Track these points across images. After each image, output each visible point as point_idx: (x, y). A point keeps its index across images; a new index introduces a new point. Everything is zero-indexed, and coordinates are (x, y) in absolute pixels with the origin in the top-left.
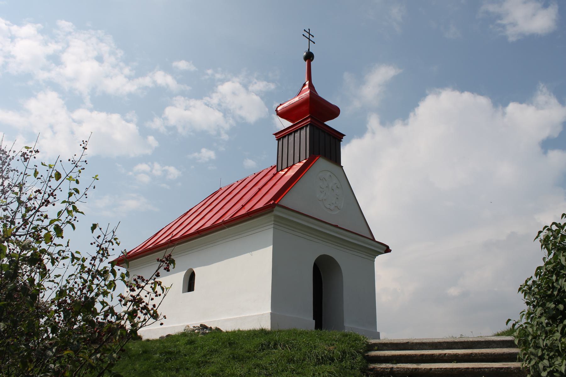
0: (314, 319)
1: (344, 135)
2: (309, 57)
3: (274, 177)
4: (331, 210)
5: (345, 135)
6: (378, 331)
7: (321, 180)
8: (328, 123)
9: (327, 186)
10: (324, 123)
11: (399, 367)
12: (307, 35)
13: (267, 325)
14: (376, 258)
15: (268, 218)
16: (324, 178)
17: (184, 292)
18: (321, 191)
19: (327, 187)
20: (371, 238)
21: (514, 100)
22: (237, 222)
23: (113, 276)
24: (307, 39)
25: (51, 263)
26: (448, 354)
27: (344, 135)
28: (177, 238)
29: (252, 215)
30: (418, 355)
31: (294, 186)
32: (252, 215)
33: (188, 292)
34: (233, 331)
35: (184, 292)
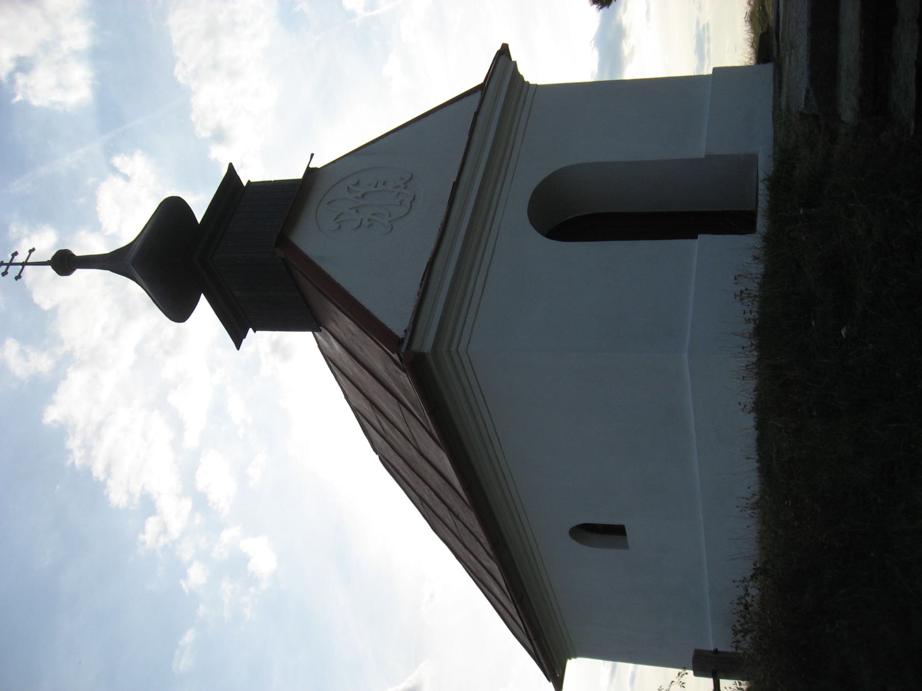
0: (696, 238)
3: (454, 509)
4: (414, 199)
7: (340, 227)
8: (199, 217)
10: (199, 223)
11: (782, 4)
12: (14, 271)
14: (528, 82)
16: (335, 220)
17: (625, 546)
18: (369, 226)
19: (357, 211)
20: (478, 95)
21: (699, 234)
25: (257, 339)
28: (505, 582)
33: (626, 535)
34: (757, 465)
35: (625, 546)
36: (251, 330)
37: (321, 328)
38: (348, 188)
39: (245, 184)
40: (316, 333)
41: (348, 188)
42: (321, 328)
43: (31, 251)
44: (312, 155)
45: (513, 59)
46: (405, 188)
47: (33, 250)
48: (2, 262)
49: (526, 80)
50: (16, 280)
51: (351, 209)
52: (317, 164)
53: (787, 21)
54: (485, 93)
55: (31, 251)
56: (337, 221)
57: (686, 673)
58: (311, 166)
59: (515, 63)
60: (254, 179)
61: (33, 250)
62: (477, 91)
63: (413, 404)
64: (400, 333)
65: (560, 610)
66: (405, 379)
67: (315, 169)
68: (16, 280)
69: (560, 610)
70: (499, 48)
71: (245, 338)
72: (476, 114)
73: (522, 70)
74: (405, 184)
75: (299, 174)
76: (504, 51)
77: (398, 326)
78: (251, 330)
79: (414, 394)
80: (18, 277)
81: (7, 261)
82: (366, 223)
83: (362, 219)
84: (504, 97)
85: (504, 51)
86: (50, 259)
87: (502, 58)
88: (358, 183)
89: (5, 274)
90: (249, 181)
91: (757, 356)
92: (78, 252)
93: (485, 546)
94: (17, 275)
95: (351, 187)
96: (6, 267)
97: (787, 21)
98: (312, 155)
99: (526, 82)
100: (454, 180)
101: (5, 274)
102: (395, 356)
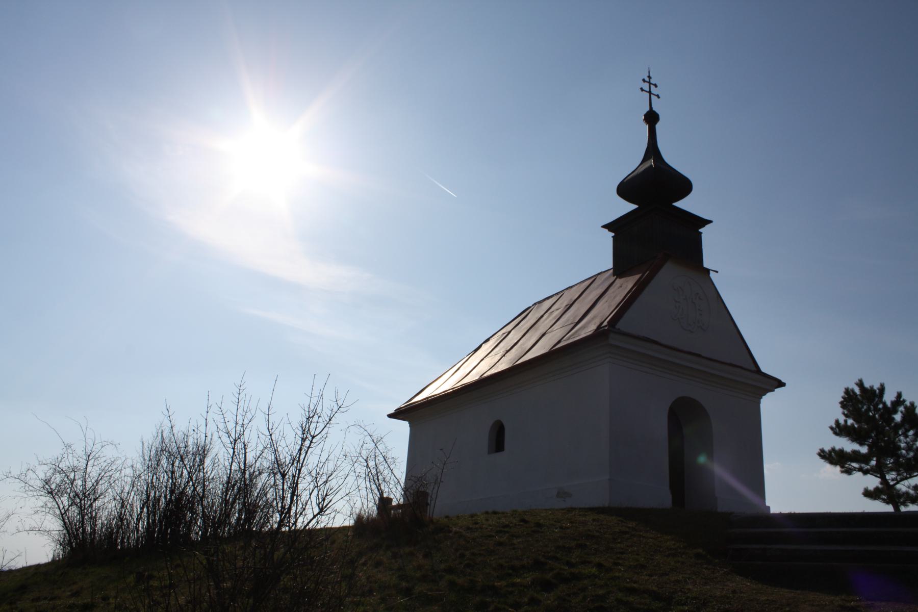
1: (705, 222)
5: (710, 222)
8: (680, 204)
12: (646, 86)
14: (762, 398)
17: (489, 453)
20: (754, 368)
27: (705, 222)
35: (489, 453)
36: (613, 234)
37: (616, 277)
39: (700, 230)
40: (612, 271)
42: (616, 277)
43: (658, 96)
44: (717, 272)
45: (777, 390)
49: (764, 397)
50: (846, 389)
52: (712, 274)
53: (297, 475)
55: (658, 96)
58: (711, 272)
59: (774, 391)
60: (703, 236)
63: (576, 332)
64: (617, 326)
66: (592, 328)
67: (709, 274)
70: (783, 381)
71: (609, 231)
72: (741, 367)
73: (769, 395)
75: (706, 264)
76: (781, 384)
77: (621, 325)
78: (613, 234)
79: (583, 335)
80: (642, 89)
85: (781, 384)
86: (654, 109)
89: (644, 81)
91: (384, 503)
92: (658, 126)
93: (489, 372)
94: (644, 88)
96: (651, 86)
97: (297, 475)
98: (717, 272)
99: (890, 503)
101: (644, 81)
102: (605, 323)
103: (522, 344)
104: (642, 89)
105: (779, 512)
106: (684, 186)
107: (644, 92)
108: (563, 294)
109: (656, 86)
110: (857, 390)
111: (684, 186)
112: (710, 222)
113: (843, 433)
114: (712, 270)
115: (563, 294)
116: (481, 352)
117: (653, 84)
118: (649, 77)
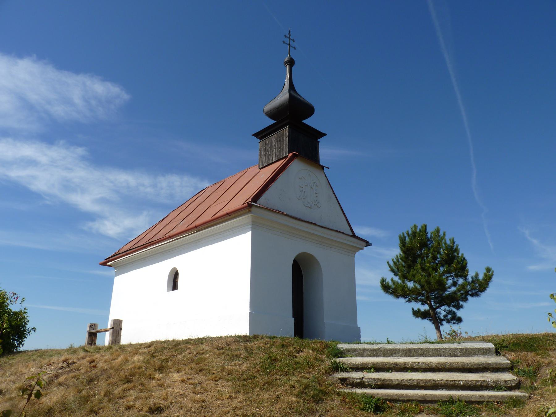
1: (322, 135)
2: (291, 62)
5: (325, 135)
6: (359, 326)
8: (306, 122)
9: (306, 184)
12: (287, 41)
13: (244, 329)
14: (356, 254)
15: (246, 218)
16: (303, 177)
17: (168, 291)
19: (306, 185)
22: (208, 225)
23: (428, 230)
24: (293, 48)
26: (421, 363)
27: (322, 135)
29: (230, 215)
30: (389, 363)
31: (264, 183)
32: (230, 215)
33: (294, 260)
38: (315, 182)
41: (315, 182)
44: (328, 168)
46: (314, 205)
47: (295, 49)
48: (291, 35)
51: (307, 183)
54: (351, 236)
56: (302, 178)
57: (23, 344)
58: (324, 167)
61: (295, 49)
62: (352, 233)
65: (330, 247)
68: (283, 42)
69: (330, 247)
74: (316, 204)
80: (284, 42)
81: (291, 38)
82: (301, 189)
83: (303, 187)
84: (371, 358)
87: (365, 244)
88: (317, 186)
89: (286, 36)
90: (319, 142)
95: (315, 183)
96: (352, 234)
98: (328, 168)
100: (317, 224)
101: (286, 36)
103: (414, 374)
104: (284, 42)
105: (246, 233)
106: (309, 110)
107: (285, 44)
108: (212, 217)
109: (294, 41)
110: (402, 236)
111: (309, 110)
112: (325, 135)
113: (394, 371)
114: (325, 167)
115: (212, 217)
116: (434, 374)
117: (291, 39)
118: (289, 34)
